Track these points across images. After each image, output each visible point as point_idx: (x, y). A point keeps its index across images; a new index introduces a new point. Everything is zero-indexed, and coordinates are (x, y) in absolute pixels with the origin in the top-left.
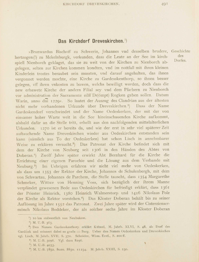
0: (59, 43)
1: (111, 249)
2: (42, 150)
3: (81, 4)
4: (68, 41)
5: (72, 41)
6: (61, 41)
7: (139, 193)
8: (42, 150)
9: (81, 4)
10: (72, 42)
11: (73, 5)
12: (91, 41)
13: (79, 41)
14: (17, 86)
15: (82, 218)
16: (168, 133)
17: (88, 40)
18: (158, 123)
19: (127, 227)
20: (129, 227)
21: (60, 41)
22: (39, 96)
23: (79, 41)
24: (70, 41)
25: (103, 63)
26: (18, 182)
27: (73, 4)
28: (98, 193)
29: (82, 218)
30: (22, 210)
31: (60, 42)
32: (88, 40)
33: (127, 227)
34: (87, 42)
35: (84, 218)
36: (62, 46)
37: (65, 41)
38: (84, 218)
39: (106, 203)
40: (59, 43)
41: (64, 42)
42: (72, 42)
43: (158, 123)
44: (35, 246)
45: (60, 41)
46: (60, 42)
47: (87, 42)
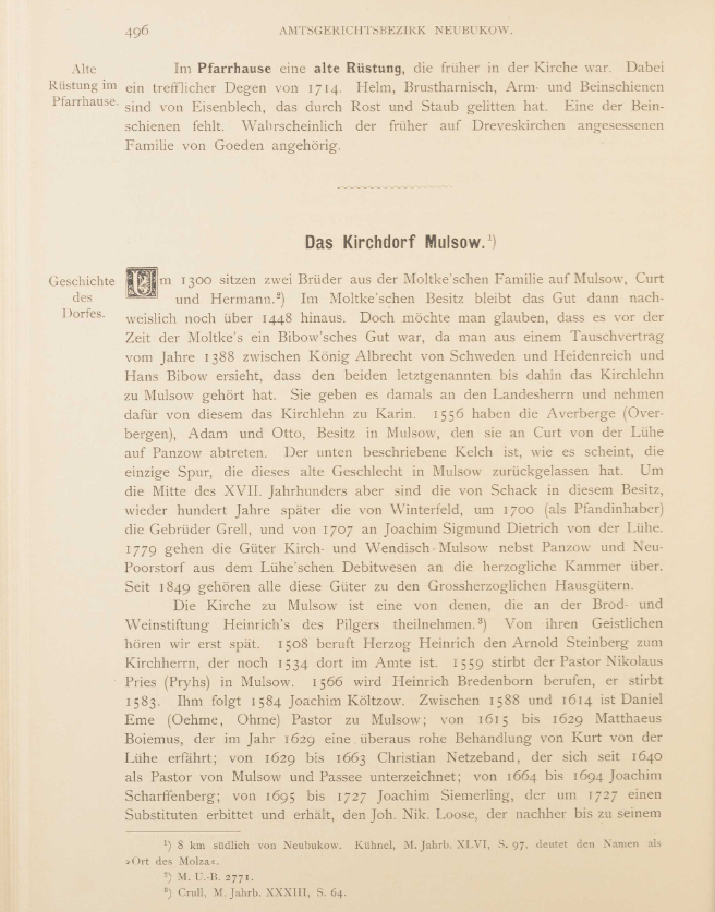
0: (308, 247)
1: (292, 892)
2: (223, 607)
3: (294, 30)
4: (338, 243)
5: (352, 242)
6: (316, 243)
7: (460, 415)
8: (223, 607)
9: (294, 30)
10: (353, 245)
11: (359, 32)
12: (420, 241)
13: (378, 242)
14: (205, 590)
15: (327, 846)
16: (660, 376)
17: (411, 239)
18: (485, 796)
19: (465, 844)
20: (472, 844)
21: (312, 242)
22: (230, 454)
23: (378, 242)
24: (346, 242)
25: (552, 739)
26: (129, 584)
27: (359, 30)
28: (256, 128)
29: (327, 846)
30: (137, 645)
31: (310, 245)
32: (411, 239)
33: (465, 844)
34: (407, 244)
35: (334, 846)
36: (318, 261)
37: (330, 244)
38: (334, 846)
39: (306, 296)
40: (308, 247)
41: (325, 244)
42: (353, 245)
43: (485, 796)
44: (182, 881)
45: (312, 242)
46: (310, 245)
47: (407, 244)
